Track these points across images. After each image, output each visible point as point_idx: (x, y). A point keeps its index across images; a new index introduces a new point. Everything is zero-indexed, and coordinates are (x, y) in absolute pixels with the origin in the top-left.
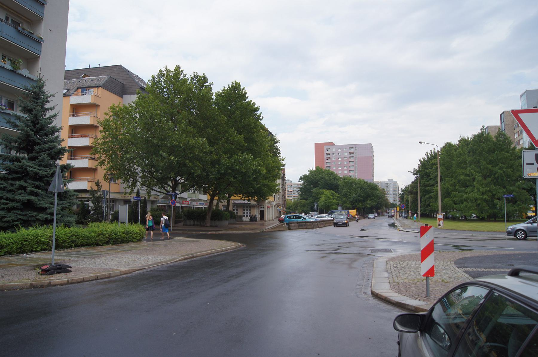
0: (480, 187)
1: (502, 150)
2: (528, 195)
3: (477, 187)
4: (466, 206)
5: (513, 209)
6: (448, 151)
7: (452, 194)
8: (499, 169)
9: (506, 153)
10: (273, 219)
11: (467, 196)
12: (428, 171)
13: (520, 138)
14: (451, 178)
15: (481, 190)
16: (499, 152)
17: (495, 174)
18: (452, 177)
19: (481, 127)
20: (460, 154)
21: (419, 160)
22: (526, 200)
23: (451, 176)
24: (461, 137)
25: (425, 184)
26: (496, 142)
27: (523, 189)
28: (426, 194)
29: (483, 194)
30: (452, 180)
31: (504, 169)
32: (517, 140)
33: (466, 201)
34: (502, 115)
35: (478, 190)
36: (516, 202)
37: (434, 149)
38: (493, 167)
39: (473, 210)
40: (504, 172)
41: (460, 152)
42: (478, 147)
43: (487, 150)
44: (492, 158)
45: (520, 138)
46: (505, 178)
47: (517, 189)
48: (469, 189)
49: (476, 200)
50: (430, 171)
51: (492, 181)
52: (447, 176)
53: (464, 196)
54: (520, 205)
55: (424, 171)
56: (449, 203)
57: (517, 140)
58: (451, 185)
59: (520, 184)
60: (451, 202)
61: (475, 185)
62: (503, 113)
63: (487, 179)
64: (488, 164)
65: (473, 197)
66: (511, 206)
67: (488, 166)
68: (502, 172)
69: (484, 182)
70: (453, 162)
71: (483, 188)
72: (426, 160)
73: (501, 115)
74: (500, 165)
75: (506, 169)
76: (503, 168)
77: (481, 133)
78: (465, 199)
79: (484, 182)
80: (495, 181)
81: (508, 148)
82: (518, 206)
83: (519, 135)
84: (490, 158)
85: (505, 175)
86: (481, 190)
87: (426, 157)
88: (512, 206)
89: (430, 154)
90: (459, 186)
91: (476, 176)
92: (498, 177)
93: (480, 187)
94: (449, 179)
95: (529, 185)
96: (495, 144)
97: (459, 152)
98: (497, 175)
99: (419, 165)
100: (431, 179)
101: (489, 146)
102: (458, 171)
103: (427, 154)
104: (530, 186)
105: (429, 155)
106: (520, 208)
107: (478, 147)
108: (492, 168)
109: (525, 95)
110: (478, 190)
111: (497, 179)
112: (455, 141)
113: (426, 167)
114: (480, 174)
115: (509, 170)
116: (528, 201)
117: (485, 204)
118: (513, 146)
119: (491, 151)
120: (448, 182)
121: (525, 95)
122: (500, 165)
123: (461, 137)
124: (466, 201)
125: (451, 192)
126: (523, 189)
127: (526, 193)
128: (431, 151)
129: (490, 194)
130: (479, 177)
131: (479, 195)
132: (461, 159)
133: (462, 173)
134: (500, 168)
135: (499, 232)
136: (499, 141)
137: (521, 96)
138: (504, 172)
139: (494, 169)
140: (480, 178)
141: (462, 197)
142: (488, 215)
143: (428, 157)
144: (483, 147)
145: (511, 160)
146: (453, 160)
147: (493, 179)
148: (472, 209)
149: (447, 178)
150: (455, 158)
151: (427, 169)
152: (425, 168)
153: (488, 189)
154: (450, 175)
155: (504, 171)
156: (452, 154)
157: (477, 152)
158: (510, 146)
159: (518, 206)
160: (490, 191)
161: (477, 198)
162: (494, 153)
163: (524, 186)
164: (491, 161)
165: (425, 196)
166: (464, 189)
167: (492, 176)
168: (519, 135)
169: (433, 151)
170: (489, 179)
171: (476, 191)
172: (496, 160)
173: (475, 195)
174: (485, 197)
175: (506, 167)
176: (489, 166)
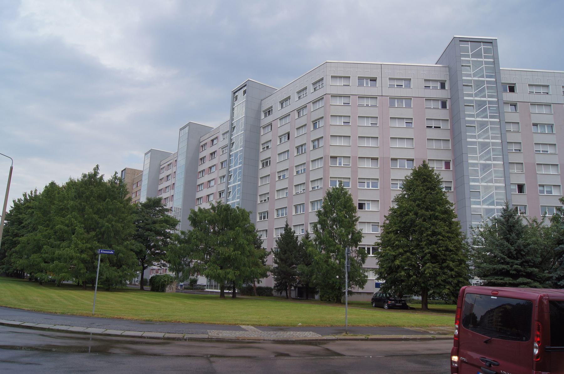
0: (79, 242)
1: (115, 199)
2: (136, 258)
3: (75, 242)
4: (57, 266)
5: (116, 274)
6: (49, 192)
7: (43, 249)
8: (107, 222)
9: (119, 203)
10: (454, 307)
11: (61, 252)
12: (20, 216)
13: (138, 188)
14: (47, 227)
15: (80, 246)
16: (111, 200)
17: (101, 227)
18: (48, 226)
19: (95, 166)
20: (64, 198)
21: (13, 201)
22: (133, 264)
23: (48, 224)
24: (70, 179)
25: (14, 234)
26: (109, 188)
27: (132, 250)
28: (13, 247)
29: (82, 252)
30: (47, 230)
31: (113, 223)
32: (135, 190)
33: (59, 259)
34: (124, 171)
35: (76, 245)
36: (121, 266)
37: (36, 190)
38: (101, 218)
39: (65, 273)
40: (112, 226)
41: (64, 194)
42: (86, 189)
43: (96, 195)
44: (101, 207)
45: (138, 188)
46: (112, 235)
47: (125, 250)
48: (65, 244)
49: (72, 258)
50: (24, 217)
51: (96, 235)
52: (42, 224)
53: (57, 252)
54: (126, 270)
55: (16, 216)
56: (36, 261)
57: (135, 190)
58: (45, 236)
59: (129, 243)
60: (39, 260)
61: (73, 239)
62: (125, 169)
63: (91, 233)
64: (95, 213)
65: (67, 255)
66: (114, 271)
67: (94, 216)
68: (110, 225)
69: (86, 235)
70: (53, 207)
71: (83, 243)
72: (23, 202)
73: (122, 171)
74: (110, 216)
75: (115, 222)
76: (112, 221)
77: (93, 173)
78: (57, 256)
79: (86, 235)
80: (100, 236)
81: (122, 197)
82: (123, 271)
83: (136, 196)
84: (99, 206)
85: (113, 230)
86: (80, 246)
87: (23, 198)
88: (116, 271)
89: (29, 195)
90: (55, 239)
91: (76, 226)
92: (104, 231)
93: (79, 242)
94: (43, 228)
95: (139, 246)
96: (107, 190)
97: (62, 195)
98: (103, 229)
99: (12, 207)
100: (24, 227)
101: (101, 192)
102: (57, 218)
103: (25, 195)
104: (140, 248)
105: (28, 196)
106: (125, 273)
107: (86, 189)
108: (99, 219)
109: (149, 154)
110: (76, 245)
111: (103, 234)
112: (61, 183)
113: (21, 210)
114: (83, 225)
115: (119, 225)
116: (135, 266)
117: (82, 265)
118: (127, 197)
119: (101, 198)
120: (40, 232)
121: (149, 154)
122: (110, 216)
123: (70, 179)
124: (59, 259)
125: (42, 246)
126: (132, 250)
127: (135, 256)
128: (31, 192)
129: (91, 253)
130: (80, 229)
131: (77, 253)
132: (64, 204)
133: (62, 222)
134: (109, 221)
135: (465, 66)
136: (113, 187)
137: (146, 154)
138: (112, 226)
139: (100, 221)
140: (82, 231)
141: (54, 253)
142: (84, 280)
143: (26, 199)
144: (92, 191)
145: (123, 213)
146: (54, 204)
147: (98, 233)
148: (63, 271)
149: (40, 227)
150: (56, 202)
151: (21, 214)
152: (19, 213)
153: (89, 246)
154: (46, 224)
155: (112, 224)
156: (54, 196)
157: (84, 196)
158: (125, 195)
159: (123, 271)
160: (91, 249)
161: (72, 256)
162: (105, 201)
163: (133, 247)
164: (99, 209)
165: (11, 249)
166: (59, 242)
167: (98, 230)
168: (136, 196)
169: (33, 193)
170: (93, 233)
171: (73, 246)
172: (106, 210)
173: (70, 251)
174: (84, 256)
175: (116, 220)
176: (96, 217)
